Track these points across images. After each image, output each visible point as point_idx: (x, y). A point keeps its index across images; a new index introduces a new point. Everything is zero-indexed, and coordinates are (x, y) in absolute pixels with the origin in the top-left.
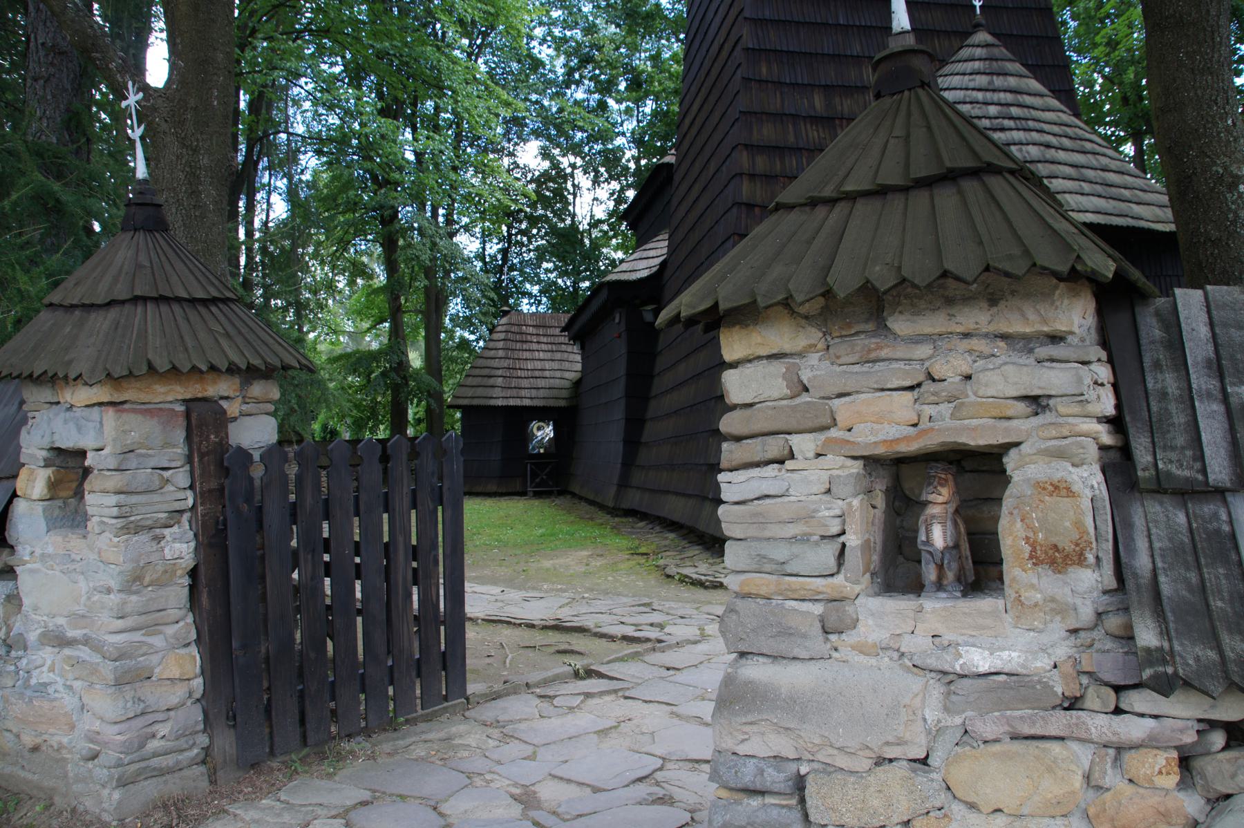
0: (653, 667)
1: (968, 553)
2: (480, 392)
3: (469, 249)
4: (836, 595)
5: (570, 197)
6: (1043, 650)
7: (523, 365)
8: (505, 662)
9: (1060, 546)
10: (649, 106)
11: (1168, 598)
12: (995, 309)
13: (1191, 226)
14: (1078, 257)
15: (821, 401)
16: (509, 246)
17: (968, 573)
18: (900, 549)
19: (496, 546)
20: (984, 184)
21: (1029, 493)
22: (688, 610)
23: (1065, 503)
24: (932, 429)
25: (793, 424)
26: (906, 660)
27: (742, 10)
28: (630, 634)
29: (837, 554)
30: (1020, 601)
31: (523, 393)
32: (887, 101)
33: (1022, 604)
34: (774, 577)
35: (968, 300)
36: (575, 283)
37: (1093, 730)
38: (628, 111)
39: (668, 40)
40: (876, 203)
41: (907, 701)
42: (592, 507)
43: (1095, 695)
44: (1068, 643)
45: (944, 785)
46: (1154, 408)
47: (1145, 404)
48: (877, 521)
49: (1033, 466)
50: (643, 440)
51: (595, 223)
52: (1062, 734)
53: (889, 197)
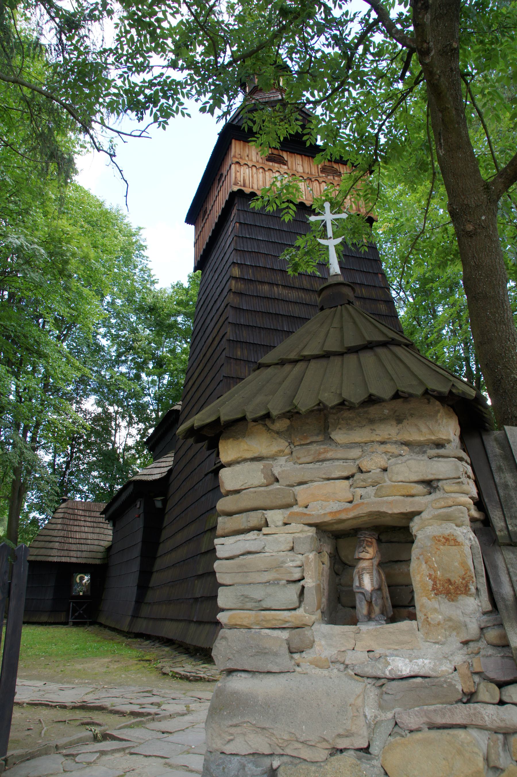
0: (152, 732)
1: (388, 595)
2: (42, 552)
3: (44, 460)
4: (298, 623)
5: (113, 431)
6: (446, 658)
7: (73, 535)
8: (41, 733)
9: (453, 580)
10: (166, 379)
12: (400, 426)
13: (503, 409)
14: (453, 385)
16: (71, 460)
17: (388, 610)
18: (339, 599)
19: (42, 656)
20: (390, 350)
21: (429, 544)
22: (177, 694)
23: (454, 549)
24: (363, 503)
25: (268, 503)
26: (350, 671)
27: (227, 318)
28: (136, 710)
29: (299, 593)
30: (428, 621)
31: (72, 554)
32: (327, 312)
33: (429, 624)
34: (254, 612)
35: (383, 420)
36: (111, 486)
37: (486, 718)
38: (153, 381)
39: (180, 342)
40: (323, 362)
41: (352, 701)
42: (113, 633)
43: (485, 689)
44: (462, 652)
45: (382, 771)
46: (502, 494)
49: (430, 527)
50: (151, 585)
51: (127, 448)
52: (465, 722)
53: (332, 358)
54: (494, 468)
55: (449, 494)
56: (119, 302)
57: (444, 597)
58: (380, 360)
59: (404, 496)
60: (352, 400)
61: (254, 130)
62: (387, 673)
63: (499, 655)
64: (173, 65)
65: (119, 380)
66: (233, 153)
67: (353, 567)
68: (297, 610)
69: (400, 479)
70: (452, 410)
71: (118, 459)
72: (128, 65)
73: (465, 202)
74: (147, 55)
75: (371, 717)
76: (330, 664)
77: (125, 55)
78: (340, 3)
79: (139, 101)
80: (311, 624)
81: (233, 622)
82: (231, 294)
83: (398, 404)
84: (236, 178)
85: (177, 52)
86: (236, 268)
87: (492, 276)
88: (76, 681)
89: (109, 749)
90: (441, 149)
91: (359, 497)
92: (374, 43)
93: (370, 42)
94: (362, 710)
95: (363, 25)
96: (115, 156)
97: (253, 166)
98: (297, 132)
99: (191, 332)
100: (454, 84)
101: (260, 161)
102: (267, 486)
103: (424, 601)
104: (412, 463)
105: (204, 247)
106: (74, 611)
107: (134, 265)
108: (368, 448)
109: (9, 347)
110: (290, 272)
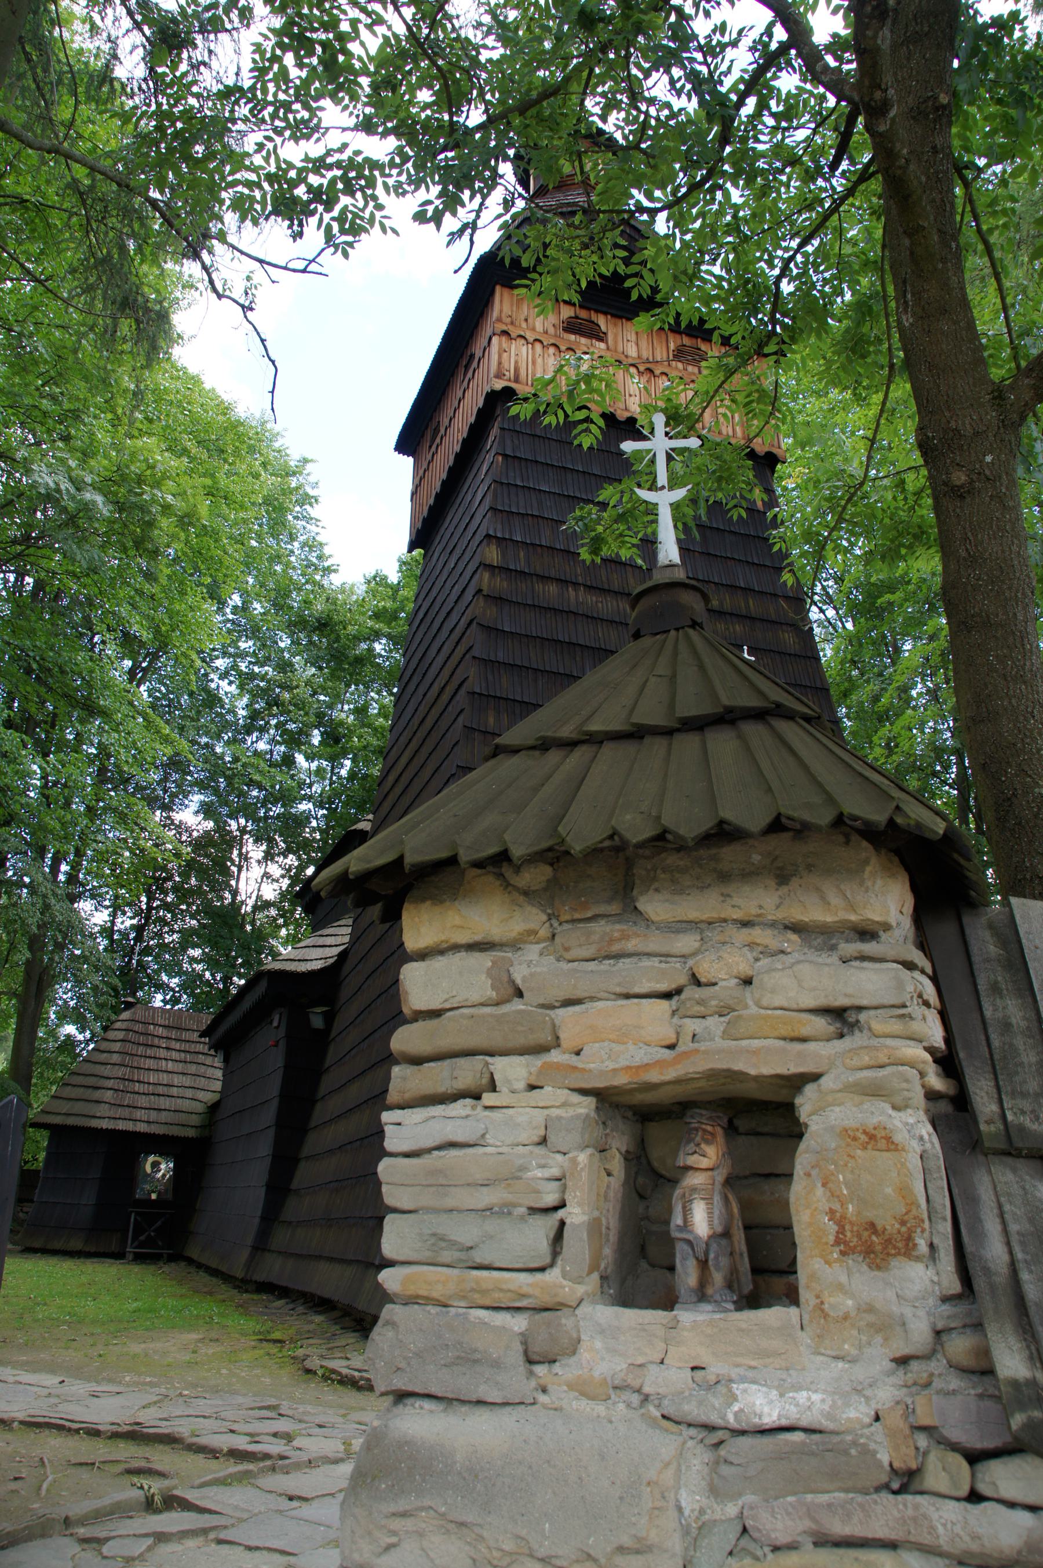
0: (269, 1496)
2: (79, 1107)
3: (94, 920)
4: (547, 1300)
5: (234, 869)
6: (858, 1392)
7: (144, 1076)
8: (40, 1488)
11: (1036, 1304)
12: (784, 889)
13: (1015, 860)
14: (898, 808)
15: (540, 1010)
16: (147, 923)
19: (65, 1322)
20: (771, 727)
21: (833, 1145)
22: (329, 1416)
24: (697, 1051)
25: (497, 1040)
26: (652, 1408)
27: (471, 648)
28: (241, 1447)
29: (552, 1235)
30: (822, 1310)
31: (139, 1114)
32: (646, 641)
33: (826, 1316)
34: (456, 1271)
35: (749, 875)
36: (227, 980)
37: (941, 1530)
38: (320, 771)
39: (378, 693)
40: (629, 748)
42: (214, 1280)
43: (940, 1466)
44: (892, 1380)
46: (996, 1043)
47: (983, 1037)
48: (611, 1194)
49: (837, 1109)
50: (294, 1185)
51: (262, 905)
52: (893, 1536)
53: (647, 740)
54: (982, 986)
55: (882, 1040)
56: (258, 607)
57: (860, 1259)
58: (748, 749)
59: (784, 1039)
60: (682, 832)
61: (525, 263)
62: (731, 1418)
63: (973, 1392)
64: (367, 126)
65: (252, 765)
66: (495, 314)
67: (674, 1182)
68: (548, 1271)
69: (777, 1004)
70: (896, 859)
71: (243, 926)
72: (277, 123)
73: (953, 424)
74: (314, 105)
75: (693, 1511)
76: (611, 1391)
77: (271, 104)
78: (707, 6)
79: (295, 200)
80: (574, 1304)
81: (412, 1290)
82: (481, 599)
83: (780, 843)
84: (500, 363)
85: (375, 99)
86: (494, 548)
87: (1003, 582)
88: (127, 1379)
89: (174, 1529)
90: (906, 312)
91: (690, 1038)
92: (779, 90)
93: (771, 89)
94: (672, 1495)
95: (757, 54)
96: (252, 309)
97: (536, 340)
98: (615, 272)
99: (398, 675)
100: (939, 180)
101: (551, 330)
102: (497, 1004)
103: (817, 1266)
104: (805, 969)
105: (431, 501)
106: (138, 1230)
107: (291, 534)
108: (714, 935)
109: (29, 689)
110: (585, 554)
